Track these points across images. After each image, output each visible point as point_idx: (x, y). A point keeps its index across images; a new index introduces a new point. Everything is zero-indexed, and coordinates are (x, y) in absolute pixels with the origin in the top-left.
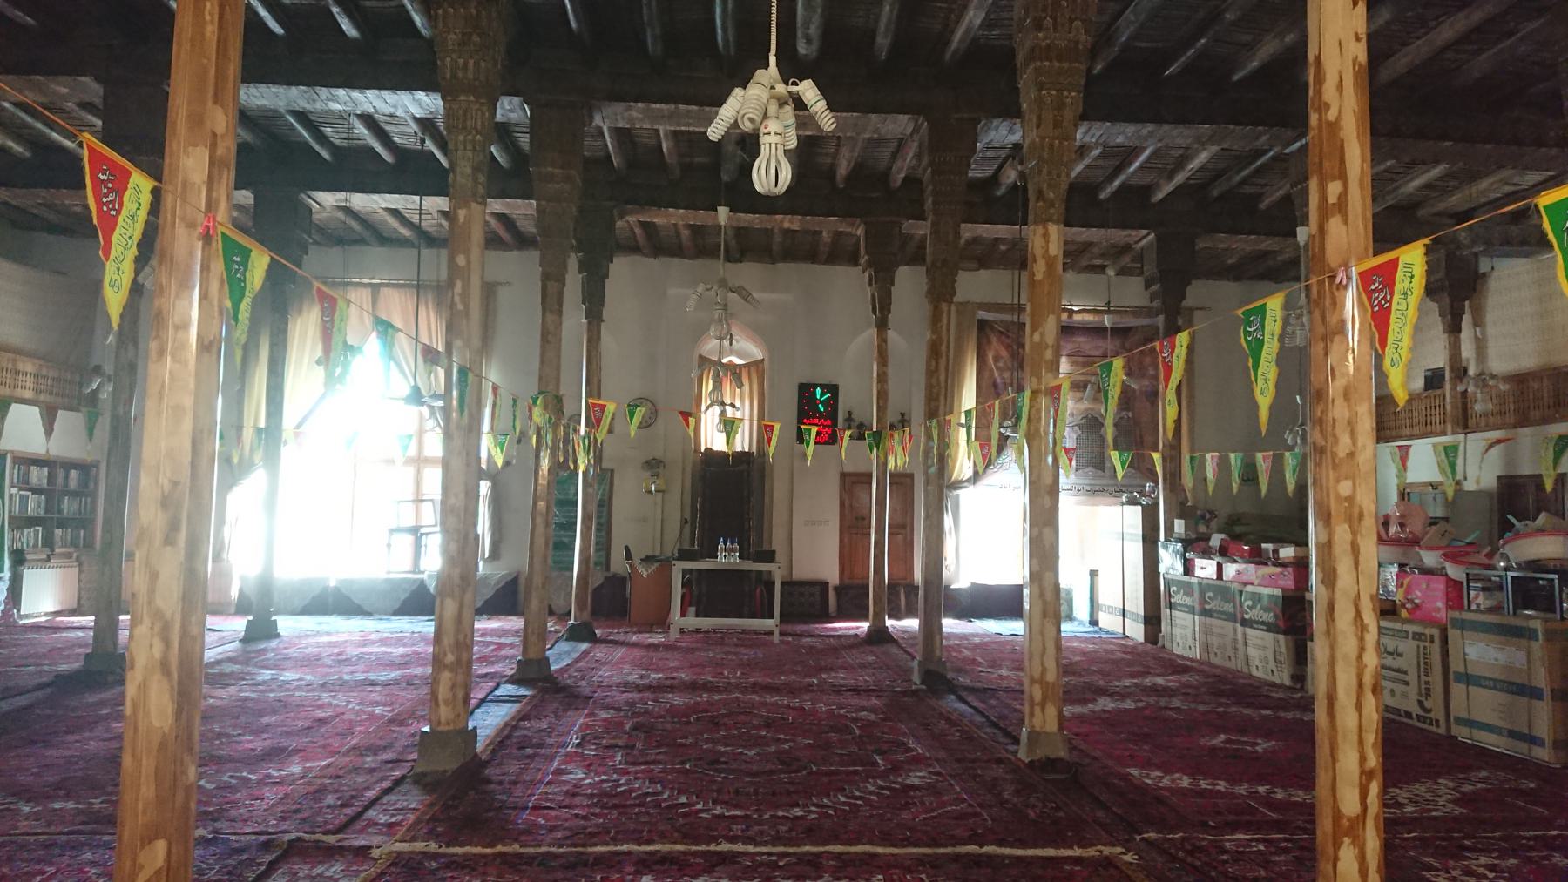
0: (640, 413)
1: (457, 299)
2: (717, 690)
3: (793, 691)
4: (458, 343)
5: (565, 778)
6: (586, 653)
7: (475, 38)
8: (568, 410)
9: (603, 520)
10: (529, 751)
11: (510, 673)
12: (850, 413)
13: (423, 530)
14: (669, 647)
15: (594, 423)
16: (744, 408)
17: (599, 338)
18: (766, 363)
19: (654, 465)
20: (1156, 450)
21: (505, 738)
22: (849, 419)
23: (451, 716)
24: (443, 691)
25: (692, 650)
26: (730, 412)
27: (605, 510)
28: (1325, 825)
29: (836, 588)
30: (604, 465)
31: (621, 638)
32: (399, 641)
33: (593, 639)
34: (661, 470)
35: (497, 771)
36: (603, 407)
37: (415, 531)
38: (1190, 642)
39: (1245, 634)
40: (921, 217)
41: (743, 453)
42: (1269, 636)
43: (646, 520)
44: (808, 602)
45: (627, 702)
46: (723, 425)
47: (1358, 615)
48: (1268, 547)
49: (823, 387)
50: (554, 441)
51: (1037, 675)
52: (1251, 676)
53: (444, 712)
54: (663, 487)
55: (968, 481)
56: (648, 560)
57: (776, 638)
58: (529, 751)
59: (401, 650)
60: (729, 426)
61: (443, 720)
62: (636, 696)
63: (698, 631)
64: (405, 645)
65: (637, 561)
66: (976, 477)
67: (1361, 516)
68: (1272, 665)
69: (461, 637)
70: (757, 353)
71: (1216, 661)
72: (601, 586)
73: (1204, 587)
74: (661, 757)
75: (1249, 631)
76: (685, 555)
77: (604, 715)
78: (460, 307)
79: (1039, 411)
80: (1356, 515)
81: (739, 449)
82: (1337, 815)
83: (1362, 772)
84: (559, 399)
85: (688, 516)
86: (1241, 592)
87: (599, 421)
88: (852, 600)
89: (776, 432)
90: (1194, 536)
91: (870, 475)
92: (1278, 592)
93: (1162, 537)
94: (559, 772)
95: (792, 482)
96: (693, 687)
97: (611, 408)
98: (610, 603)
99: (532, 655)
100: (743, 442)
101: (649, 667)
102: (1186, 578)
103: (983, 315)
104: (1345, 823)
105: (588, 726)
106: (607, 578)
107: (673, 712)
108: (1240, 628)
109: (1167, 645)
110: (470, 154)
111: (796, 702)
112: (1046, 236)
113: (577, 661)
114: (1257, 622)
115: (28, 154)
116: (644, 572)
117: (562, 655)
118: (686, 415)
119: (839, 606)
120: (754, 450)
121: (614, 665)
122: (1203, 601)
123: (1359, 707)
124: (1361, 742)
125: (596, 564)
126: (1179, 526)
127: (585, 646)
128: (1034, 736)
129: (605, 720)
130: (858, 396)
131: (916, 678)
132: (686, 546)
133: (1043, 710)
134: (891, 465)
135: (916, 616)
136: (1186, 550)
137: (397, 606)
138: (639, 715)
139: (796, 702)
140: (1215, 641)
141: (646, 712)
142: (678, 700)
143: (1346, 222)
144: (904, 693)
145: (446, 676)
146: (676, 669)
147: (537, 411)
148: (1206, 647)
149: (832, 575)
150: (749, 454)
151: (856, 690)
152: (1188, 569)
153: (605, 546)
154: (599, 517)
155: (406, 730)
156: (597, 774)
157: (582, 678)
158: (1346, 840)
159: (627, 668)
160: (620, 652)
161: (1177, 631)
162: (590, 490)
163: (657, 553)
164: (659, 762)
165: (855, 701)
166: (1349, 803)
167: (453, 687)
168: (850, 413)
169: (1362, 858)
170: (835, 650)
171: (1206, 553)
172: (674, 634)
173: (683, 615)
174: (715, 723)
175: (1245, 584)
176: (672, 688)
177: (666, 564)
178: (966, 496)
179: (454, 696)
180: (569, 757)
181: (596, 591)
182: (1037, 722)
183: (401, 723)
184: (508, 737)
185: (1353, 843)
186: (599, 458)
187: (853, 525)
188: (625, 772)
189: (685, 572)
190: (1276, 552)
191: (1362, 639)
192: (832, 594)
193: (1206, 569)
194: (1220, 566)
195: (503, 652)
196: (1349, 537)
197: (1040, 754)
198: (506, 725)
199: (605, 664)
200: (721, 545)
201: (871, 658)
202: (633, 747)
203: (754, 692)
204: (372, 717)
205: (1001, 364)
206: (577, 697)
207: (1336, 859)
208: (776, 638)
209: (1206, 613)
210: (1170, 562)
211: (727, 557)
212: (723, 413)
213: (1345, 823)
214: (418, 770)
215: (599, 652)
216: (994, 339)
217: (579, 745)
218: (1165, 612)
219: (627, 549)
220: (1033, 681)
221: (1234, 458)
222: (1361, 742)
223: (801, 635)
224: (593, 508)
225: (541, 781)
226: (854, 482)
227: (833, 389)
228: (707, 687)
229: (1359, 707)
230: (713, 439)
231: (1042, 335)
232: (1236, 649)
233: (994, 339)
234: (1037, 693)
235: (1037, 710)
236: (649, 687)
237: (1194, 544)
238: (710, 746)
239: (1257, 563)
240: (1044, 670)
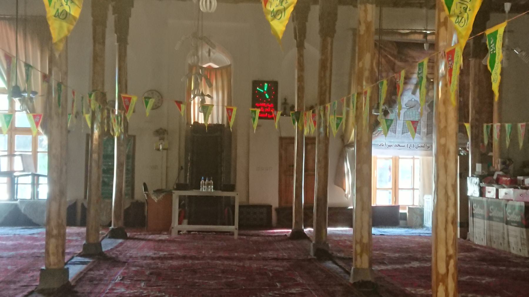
0: (151, 102)
2: (198, 259)
3: (240, 259)
4: (54, 70)
5: (115, 291)
6: (121, 244)
8: (109, 98)
9: (129, 167)
10: (95, 282)
11: (79, 252)
12: (285, 100)
13: (15, 174)
14: (169, 241)
15: (124, 108)
16: (216, 99)
17: (125, 55)
18: (232, 67)
19: (161, 133)
20: (467, 122)
21: (81, 278)
22: (285, 103)
23: (56, 261)
24: (52, 248)
25: (185, 242)
26: (208, 101)
27: (130, 161)
28: (434, 278)
29: (277, 210)
30: (130, 133)
31: (142, 237)
32: (8, 239)
33: (125, 238)
34: (166, 136)
35: (80, 289)
36: (130, 99)
37: (10, 174)
38: (501, 241)
39: (508, 230)
41: (218, 125)
42: (518, 229)
43: (157, 167)
44: (257, 217)
45: (146, 264)
46: (206, 108)
47: (446, 192)
48: (520, 178)
49: (268, 82)
50: (102, 118)
51: (358, 240)
52: (510, 253)
53: (53, 259)
54: (167, 146)
56: (158, 191)
57: (236, 236)
58: (95, 282)
59: (11, 243)
60: (205, 109)
61: (52, 263)
62: (152, 262)
63: (189, 232)
64: (12, 240)
65: (151, 192)
67: (448, 152)
68: (520, 247)
69: (60, 221)
70: (227, 61)
71: (494, 246)
72: (128, 209)
73: (490, 202)
74: (165, 284)
75: (510, 227)
76: (180, 187)
77: (134, 269)
79: (362, 104)
80: (447, 152)
81: (215, 122)
82: (438, 273)
83: (447, 256)
84: (104, 95)
85: (183, 164)
86: (506, 205)
87: (127, 107)
88: (284, 217)
89: (234, 112)
90: (486, 173)
91: (293, 139)
92: (523, 204)
93: (470, 175)
94: (112, 289)
96: (184, 258)
97: (134, 99)
98: (135, 218)
99: (92, 240)
100: (216, 117)
101: (159, 249)
102: (481, 198)
104: (440, 277)
105: (125, 273)
106: (132, 203)
107: (171, 268)
108: (505, 226)
109: (471, 239)
111: (241, 264)
112: (366, 11)
113: (116, 247)
114: (513, 222)
116: (155, 199)
117: (108, 245)
118: (179, 103)
119: (279, 219)
120: (225, 123)
121: (139, 249)
122: (489, 212)
123: (446, 229)
124: (446, 244)
125: (126, 195)
126: (479, 166)
127: (120, 241)
128: (357, 270)
129: (134, 271)
130: (288, 90)
131: (312, 253)
132: (182, 181)
133: (361, 256)
134: (305, 133)
135: (312, 226)
136: (481, 181)
138: (153, 269)
139: (241, 264)
140: (494, 234)
141: (157, 268)
142: (175, 263)
143: (446, 29)
144: (304, 260)
145: (53, 241)
146: (175, 250)
147: (93, 102)
148: (490, 239)
149: (275, 203)
150: (222, 126)
151: (276, 259)
152: (482, 193)
153: (131, 184)
154: (127, 166)
155: (28, 275)
156: (131, 289)
157: (121, 254)
158: (441, 284)
159: (146, 250)
160: (142, 243)
161: (476, 230)
162: (122, 148)
163: (164, 187)
164: (164, 286)
165: (275, 263)
166: (442, 270)
167: (57, 247)
168: (285, 100)
169: (446, 290)
170: (270, 243)
171: (490, 184)
172: (174, 234)
173: (180, 223)
174: (194, 271)
175: (508, 200)
176: (172, 258)
177: (169, 194)
179: (58, 251)
180: (116, 284)
181: (127, 211)
182: (359, 264)
183: (24, 272)
184: (83, 277)
185: (443, 284)
186: (126, 128)
187: (286, 170)
188: (145, 289)
189: (181, 198)
190: (523, 181)
191: (447, 202)
192: (274, 214)
193: (491, 192)
194: (497, 191)
195: (72, 244)
196: (443, 161)
197: (359, 278)
198: (81, 273)
199: (134, 248)
200: (202, 182)
201: (290, 246)
202: (150, 281)
203: (218, 260)
204: (6, 270)
206: (119, 262)
207: (437, 292)
208: (236, 236)
209: (490, 218)
210: (473, 189)
211: (206, 188)
212: (203, 101)
213: (440, 277)
214: (40, 288)
215: (129, 243)
217: (121, 280)
218: (471, 219)
219: (145, 184)
220: (357, 243)
221: (507, 126)
222: (446, 244)
223: (253, 235)
224: (124, 159)
225: (103, 292)
226: (286, 143)
227: (274, 86)
228: (191, 258)
229: (446, 229)
230: (198, 117)
231: (363, 63)
232: (504, 238)
234: (359, 250)
235: (358, 257)
236: (159, 258)
237: (486, 178)
238: (191, 280)
239: (515, 188)
240: (362, 237)
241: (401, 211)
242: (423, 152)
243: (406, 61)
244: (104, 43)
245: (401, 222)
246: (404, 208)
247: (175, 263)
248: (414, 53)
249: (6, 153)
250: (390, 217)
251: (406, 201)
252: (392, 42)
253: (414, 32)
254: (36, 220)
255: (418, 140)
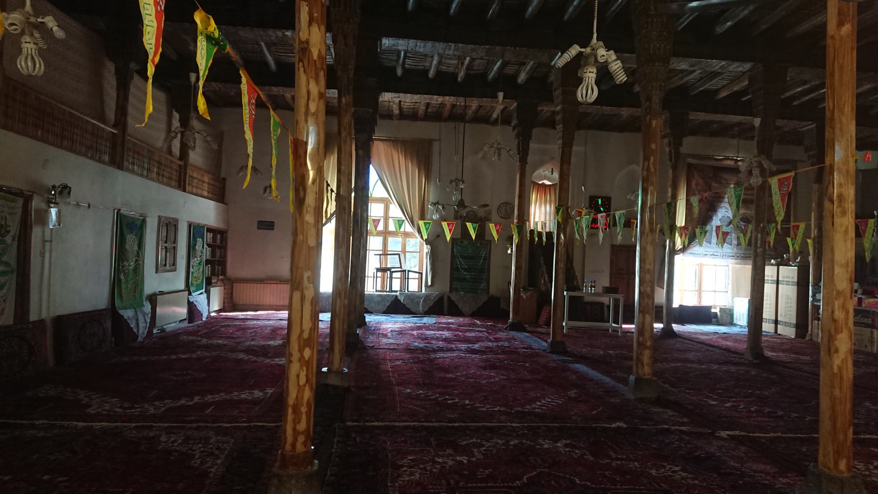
1: (651, 166)
7: (665, 34)
20: (810, 238)
40: (550, 100)
44: (596, 312)
49: (602, 198)
55: (680, 250)
66: (684, 249)
78: (653, 170)
95: (584, 252)
103: (690, 160)
110: (658, 92)
115: (566, 17)
135: (662, 322)
137: (385, 309)
178: (678, 259)
205: (699, 188)
216: (696, 174)
233: (696, 174)
241: (713, 310)
242: (734, 261)
243: (720, 183)
244: (569, 164)
245: (714, 320)
246: (715, 308)
247: (733, 369)
248: (726, 176)
249: (381, 253)
250: (701, 315)
251: (715, 301)
252: (711, 166)
253: (727, 159)
254: (413, 310)
255: (727, 249)
